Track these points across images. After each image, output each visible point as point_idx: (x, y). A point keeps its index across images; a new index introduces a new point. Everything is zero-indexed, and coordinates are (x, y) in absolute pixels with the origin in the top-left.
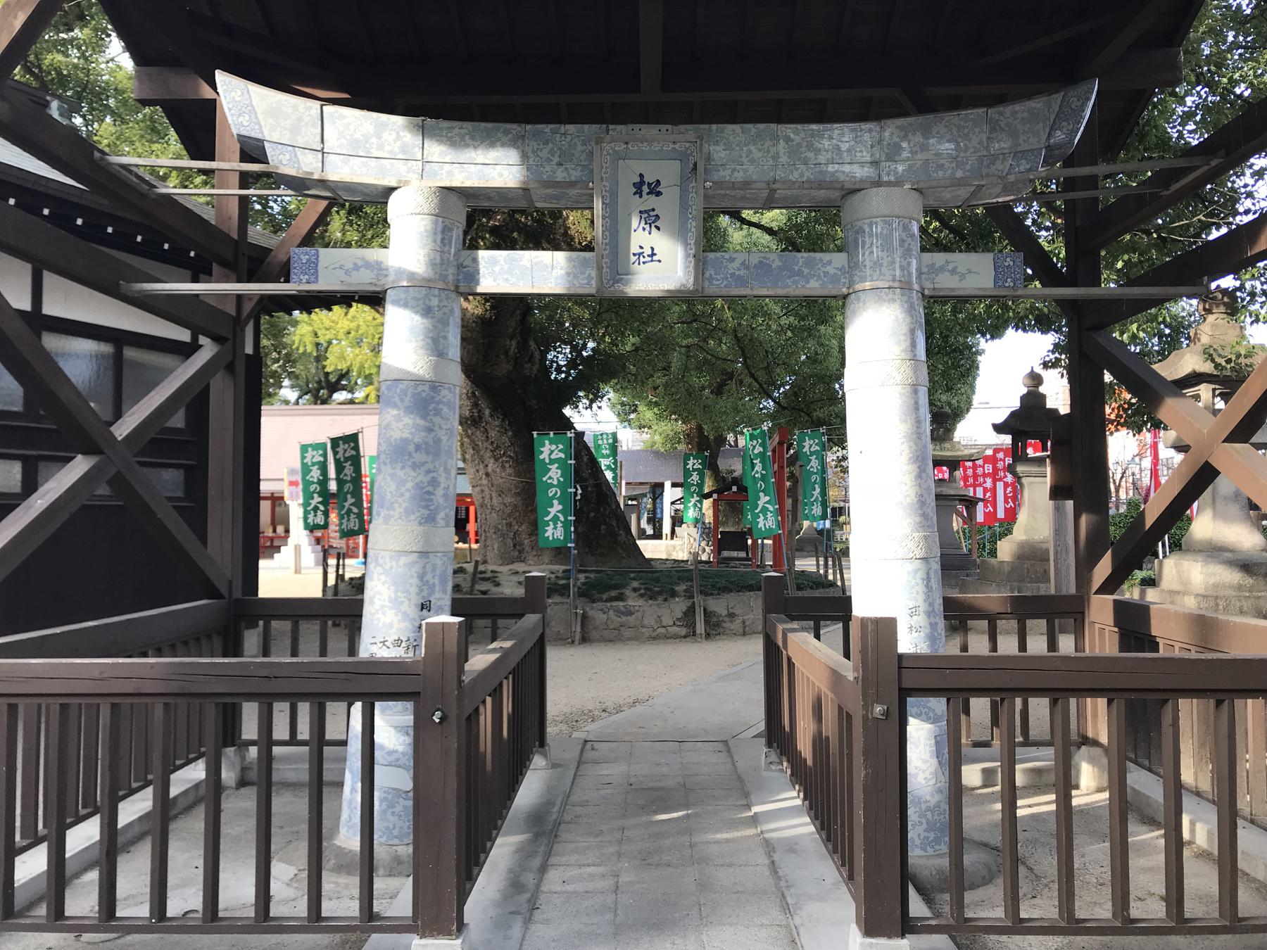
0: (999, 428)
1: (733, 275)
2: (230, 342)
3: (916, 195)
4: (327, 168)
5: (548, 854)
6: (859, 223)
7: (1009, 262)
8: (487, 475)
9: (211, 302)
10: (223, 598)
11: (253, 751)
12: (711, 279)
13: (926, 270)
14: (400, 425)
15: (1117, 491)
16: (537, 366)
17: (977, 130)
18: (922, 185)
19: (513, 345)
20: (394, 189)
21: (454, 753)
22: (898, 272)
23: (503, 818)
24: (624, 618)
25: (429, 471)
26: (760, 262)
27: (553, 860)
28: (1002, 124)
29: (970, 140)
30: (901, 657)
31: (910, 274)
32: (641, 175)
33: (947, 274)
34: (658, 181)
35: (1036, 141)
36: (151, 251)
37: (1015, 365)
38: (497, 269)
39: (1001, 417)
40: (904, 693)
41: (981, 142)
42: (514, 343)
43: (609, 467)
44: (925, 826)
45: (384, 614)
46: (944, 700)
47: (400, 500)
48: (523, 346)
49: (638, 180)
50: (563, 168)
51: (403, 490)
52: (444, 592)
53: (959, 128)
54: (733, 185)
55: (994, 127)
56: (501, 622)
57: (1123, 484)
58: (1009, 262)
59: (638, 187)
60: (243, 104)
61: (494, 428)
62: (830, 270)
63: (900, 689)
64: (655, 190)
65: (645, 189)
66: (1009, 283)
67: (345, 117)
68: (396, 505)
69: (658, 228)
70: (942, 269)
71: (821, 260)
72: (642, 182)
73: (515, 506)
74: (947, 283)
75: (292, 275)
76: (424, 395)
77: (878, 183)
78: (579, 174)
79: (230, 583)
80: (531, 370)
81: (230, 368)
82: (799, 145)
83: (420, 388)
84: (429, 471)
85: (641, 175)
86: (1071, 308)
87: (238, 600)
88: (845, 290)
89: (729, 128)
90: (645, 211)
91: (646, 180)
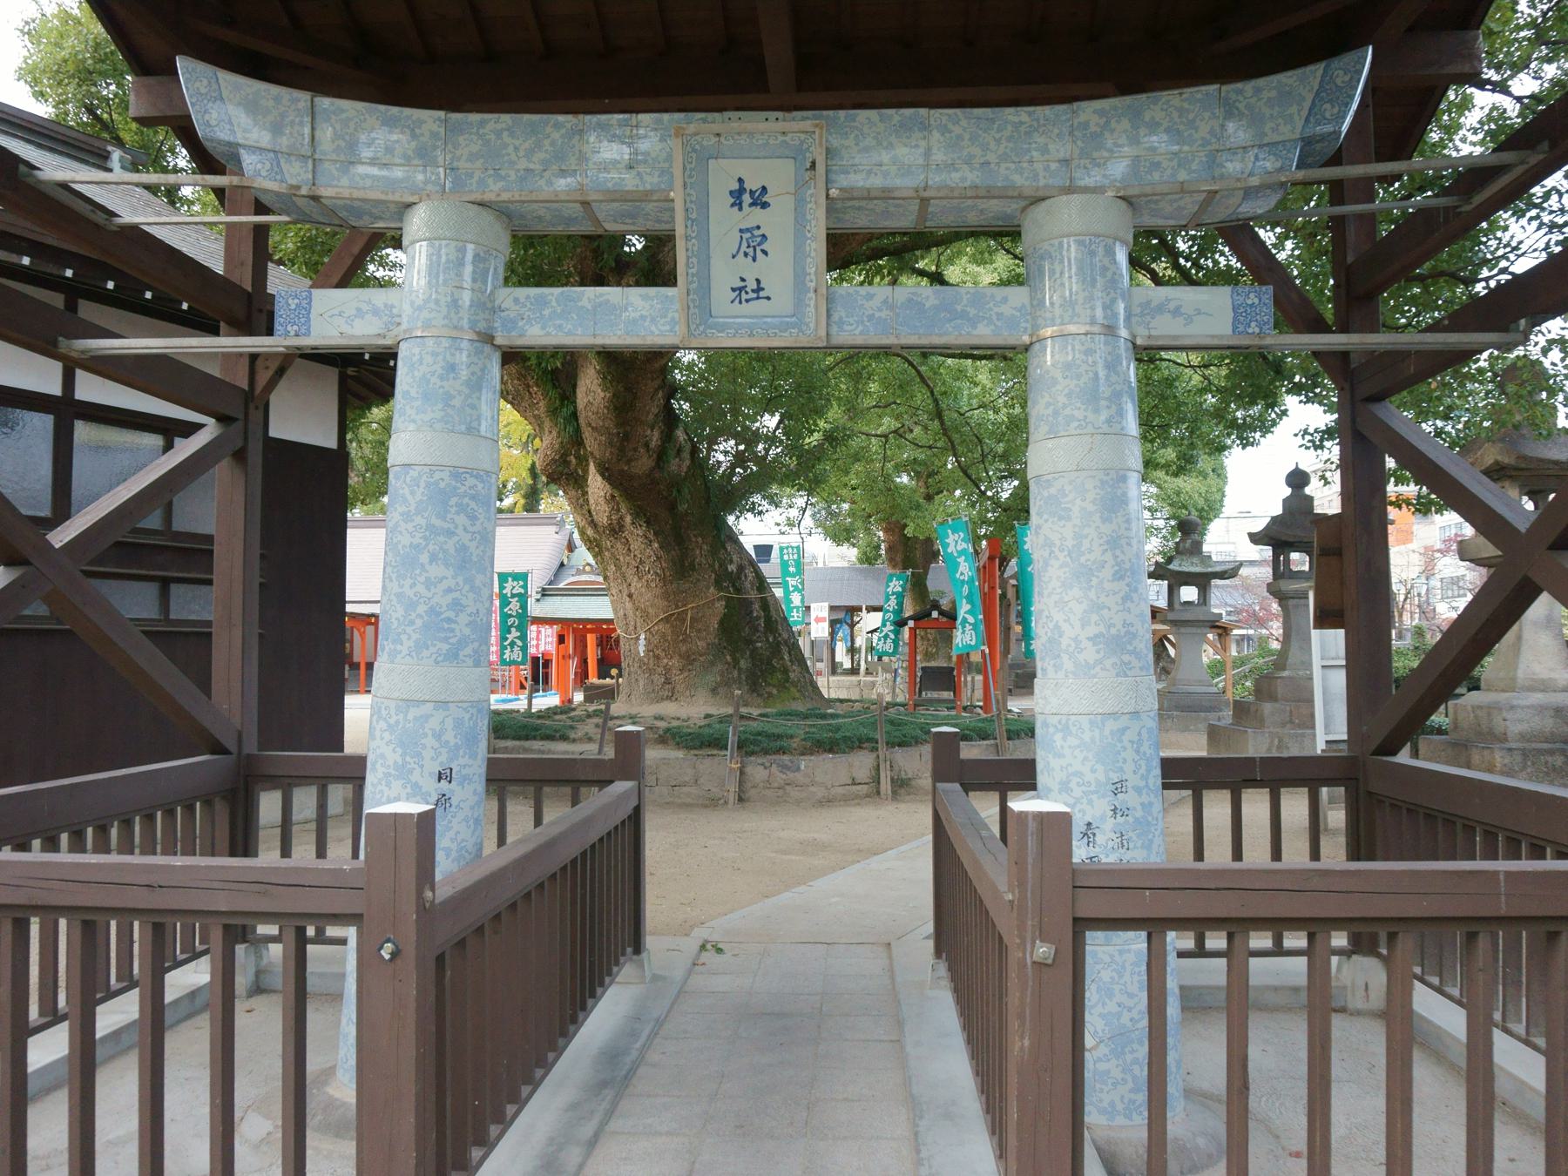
0: (1255, 538)
1: (871, 317)
2: (239, 425)
3: (1123, 205)
4: (321, 180)
5: (610, 1114)
6: (1046, 246)
7: (1253, 299)
8: (630, 596)
9: (215, 370)
10: (225, 752)
11: (276, 950)
12: (841, 322)
13: (1138, 310)
14: (410, 526)
15: (1401, 616)
16: (688, 462)
17: (1207, 115)
18: (1130, 192)
19: (655, 438)
20: (409, 206)
21: (412, 1005)
22: (1099, 313)
23: (548, 1067)
24: (791, 775)
25: (449, 590)
26: (910, 300)
27: (614, 1125)
28: (1241, 106)
29: (1196, 129)
30: (1075, 872)
31: (1115, 315)
32: (740, 180)
33: (1168, 316)
34: (764, 188)
35: (1290, 127)
36: (128, 301)
37: (1281, 459)
38: (546, 312)
39: (1259, 525)
40: (1082, 925)
41: (1212, 132)
42: (656, 434)
43: (796, 589)
44: (1130, 1085)
45: (388, 785)
46: (1144, 934)
47: (409, 630)
48: (668, 436)
49: (736, 186)
50: (634, 172)
51: (414, 615)
52: (474, 756)
53: (1181, 111)
54: (868, 196)
55: (1230, 112)
56: (583, 790)
57: (1407, 606)
58: (1253, 299)
59: (737, 195)
60: (225, 104)
61: (636, 535)
62: (1006, 310)
63: (1076, 920)
64: (760, 202)
65: (747, 199)
66: (1253, 328)
67: (343, 111)
68: (404, 637)
69: (765, 252)
70: (1160, 309)
71: (992, 296)
72: (741, 190)
73: (664, 635)
74: (1164, 328)
75: (277, 326)
76: (442, 485)
77: (1070, 190)
78: (656, 180)
79: (240, 734)
80: (679, 466)
81: (240, 456)
82: (960, 137)
83: (437, 475)
84: (449, 590)
85: (740, 180)
86: (1339, 365)
87: (249, 756)
88: (1026, 339)
89: (863, 114)
90: (748, 230)
91: (747, 186)
